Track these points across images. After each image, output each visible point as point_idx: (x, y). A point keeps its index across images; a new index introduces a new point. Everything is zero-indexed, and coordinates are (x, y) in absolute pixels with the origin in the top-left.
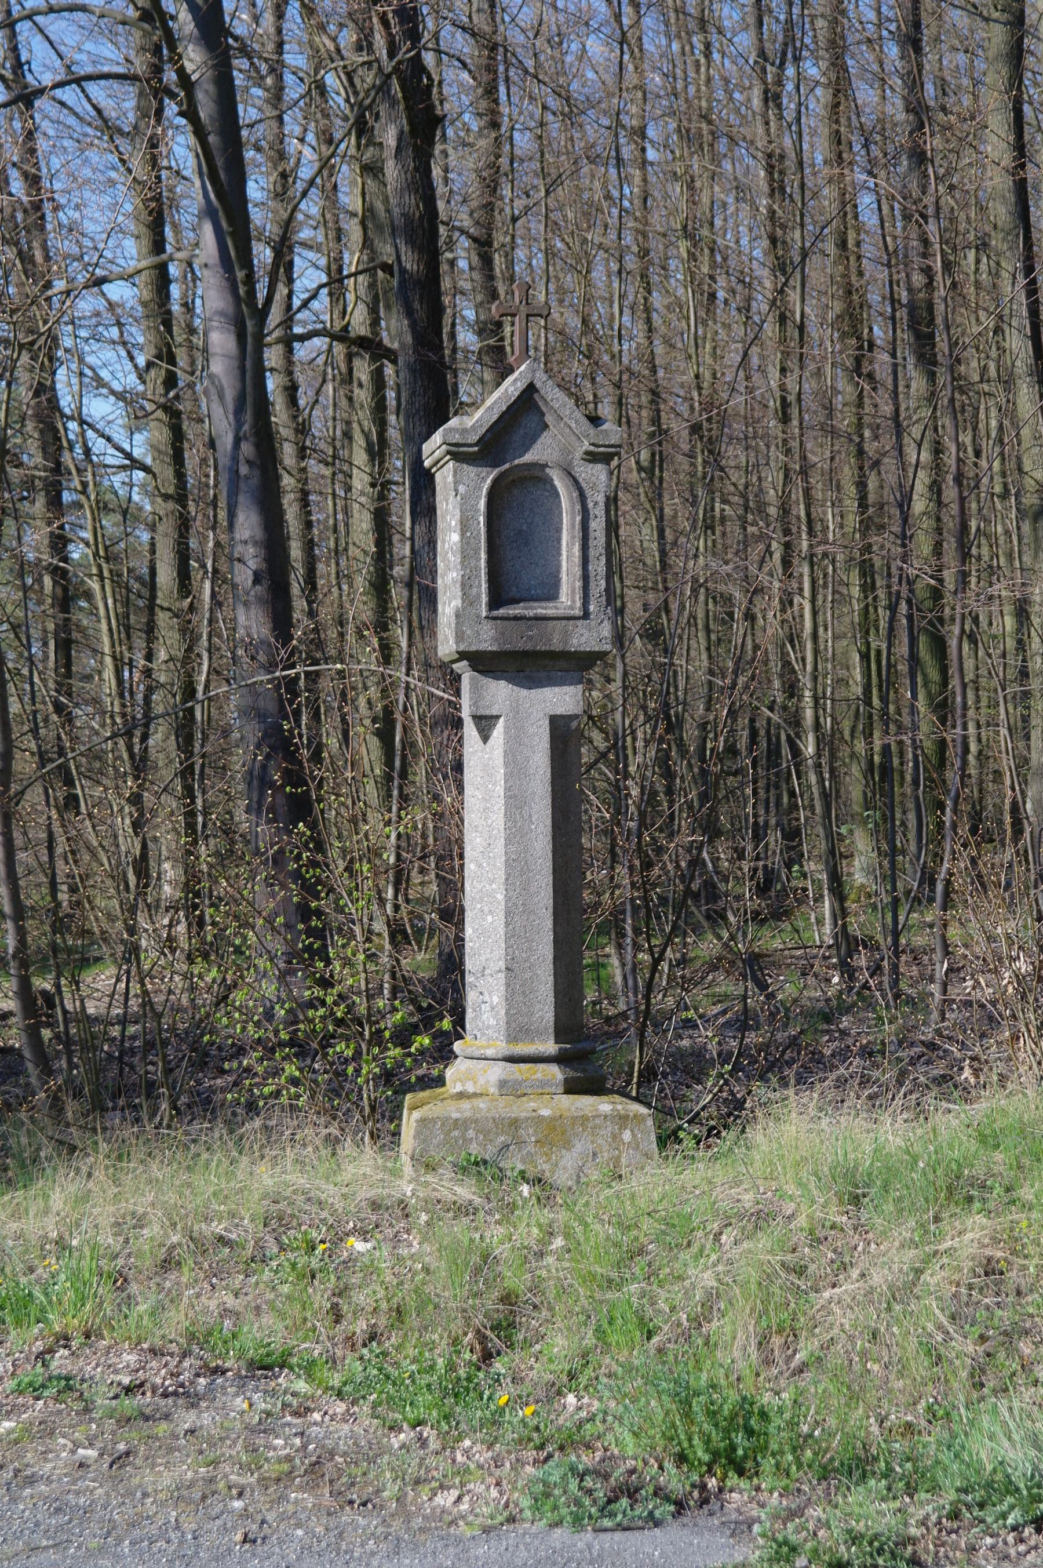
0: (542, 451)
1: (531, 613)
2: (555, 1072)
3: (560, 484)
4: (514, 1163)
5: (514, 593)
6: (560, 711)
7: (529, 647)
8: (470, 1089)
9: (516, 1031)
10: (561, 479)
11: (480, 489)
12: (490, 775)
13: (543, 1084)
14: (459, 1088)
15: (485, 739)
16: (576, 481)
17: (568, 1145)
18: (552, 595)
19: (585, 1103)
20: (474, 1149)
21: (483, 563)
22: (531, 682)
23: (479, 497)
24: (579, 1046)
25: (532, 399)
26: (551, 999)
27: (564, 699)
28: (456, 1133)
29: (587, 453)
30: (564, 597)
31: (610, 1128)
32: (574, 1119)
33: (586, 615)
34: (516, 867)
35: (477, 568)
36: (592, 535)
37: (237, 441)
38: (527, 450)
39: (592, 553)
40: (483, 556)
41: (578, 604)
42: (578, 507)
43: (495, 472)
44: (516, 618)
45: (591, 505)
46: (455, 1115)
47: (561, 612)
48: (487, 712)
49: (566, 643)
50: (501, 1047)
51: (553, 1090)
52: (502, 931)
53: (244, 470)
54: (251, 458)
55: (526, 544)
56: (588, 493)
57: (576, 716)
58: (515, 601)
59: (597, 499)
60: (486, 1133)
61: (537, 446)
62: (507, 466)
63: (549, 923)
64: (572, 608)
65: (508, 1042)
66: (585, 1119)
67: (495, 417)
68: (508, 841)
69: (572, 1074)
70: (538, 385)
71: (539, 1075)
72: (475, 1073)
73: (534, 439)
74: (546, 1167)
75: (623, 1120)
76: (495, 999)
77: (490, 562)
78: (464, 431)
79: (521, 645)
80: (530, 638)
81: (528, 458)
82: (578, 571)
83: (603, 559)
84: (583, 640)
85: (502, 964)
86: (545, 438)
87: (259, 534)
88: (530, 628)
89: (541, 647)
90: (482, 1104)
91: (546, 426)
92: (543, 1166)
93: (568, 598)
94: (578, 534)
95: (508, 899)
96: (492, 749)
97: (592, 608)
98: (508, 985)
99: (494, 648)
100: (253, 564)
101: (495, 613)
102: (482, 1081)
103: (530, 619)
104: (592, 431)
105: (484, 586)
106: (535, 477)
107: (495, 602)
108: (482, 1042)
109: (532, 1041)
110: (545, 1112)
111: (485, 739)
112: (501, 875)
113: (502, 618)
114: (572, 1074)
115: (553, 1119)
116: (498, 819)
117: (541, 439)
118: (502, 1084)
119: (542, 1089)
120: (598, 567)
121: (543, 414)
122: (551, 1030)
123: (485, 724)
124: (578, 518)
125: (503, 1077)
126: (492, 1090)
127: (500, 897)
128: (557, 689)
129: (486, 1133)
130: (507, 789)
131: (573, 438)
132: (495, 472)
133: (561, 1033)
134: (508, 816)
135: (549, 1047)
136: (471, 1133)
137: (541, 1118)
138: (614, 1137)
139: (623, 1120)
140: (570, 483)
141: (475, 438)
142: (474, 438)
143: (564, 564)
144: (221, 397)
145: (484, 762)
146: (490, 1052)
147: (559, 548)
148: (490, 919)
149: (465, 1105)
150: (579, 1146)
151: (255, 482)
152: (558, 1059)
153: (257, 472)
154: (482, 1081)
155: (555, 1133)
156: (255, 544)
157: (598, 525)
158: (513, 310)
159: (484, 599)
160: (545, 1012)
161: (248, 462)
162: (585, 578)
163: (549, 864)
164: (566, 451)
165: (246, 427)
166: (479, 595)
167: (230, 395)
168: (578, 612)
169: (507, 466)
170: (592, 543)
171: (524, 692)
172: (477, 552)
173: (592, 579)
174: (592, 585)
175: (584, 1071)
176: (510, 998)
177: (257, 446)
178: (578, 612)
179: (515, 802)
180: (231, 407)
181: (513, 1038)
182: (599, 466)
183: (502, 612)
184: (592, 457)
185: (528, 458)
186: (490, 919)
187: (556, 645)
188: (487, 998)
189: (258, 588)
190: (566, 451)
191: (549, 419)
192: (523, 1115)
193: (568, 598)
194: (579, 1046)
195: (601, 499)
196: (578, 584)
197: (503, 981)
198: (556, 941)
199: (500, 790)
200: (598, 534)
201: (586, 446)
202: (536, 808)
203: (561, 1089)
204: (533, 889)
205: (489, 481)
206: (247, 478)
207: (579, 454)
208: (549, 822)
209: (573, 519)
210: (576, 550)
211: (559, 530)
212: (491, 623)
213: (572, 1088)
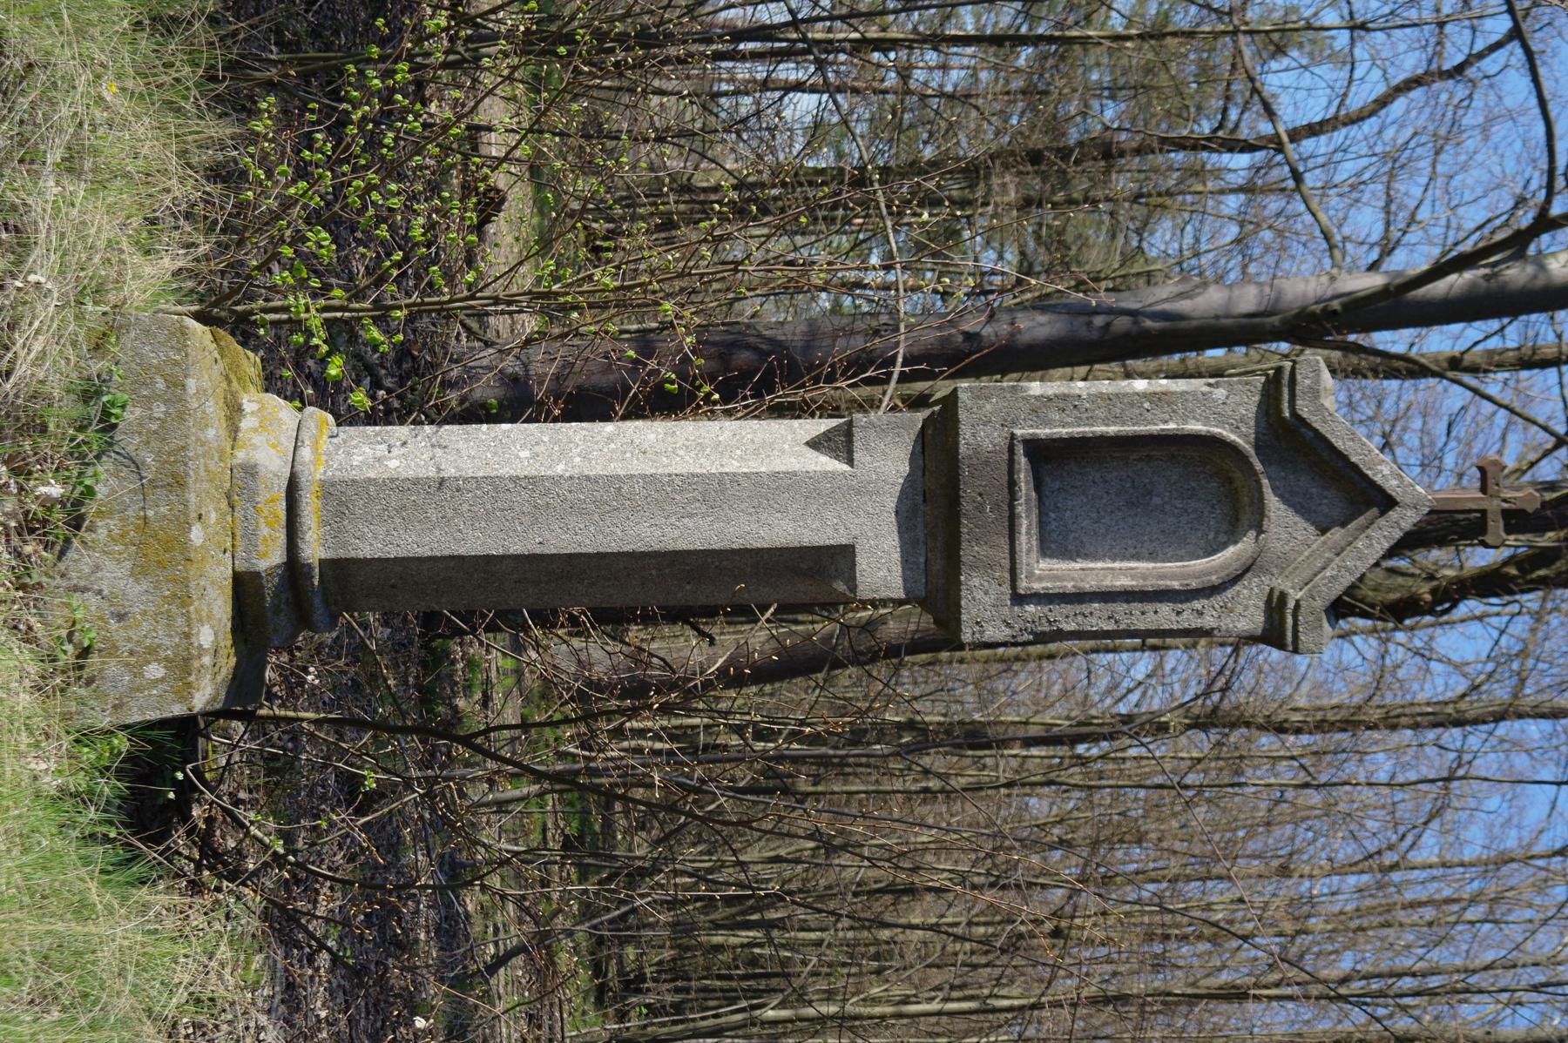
0: (1283, 523)
1: (1020, 509)
2: (271, 557)
3: (1230, 555)
4: (106, 481)
5: (1051, 484)
6: (862, 562)
7: (966, 506)
8: (246, 424)
9: (339, 496)
10: (1238, 556)
11: (1220, 424)
12: (756, 452)
13: (251, 536)
14: (248, 407)
15: (814, 444)
16: (1236, 579)
17: (139, 572)
18: (1046, 550)
19: (220, 606)
20: (132, 415)
21: (1100, 429)
22: (907, 515)
23: (1206, 422)
24: (317, 601)
25: (1368, 507)
26: (393, 553)
27: (881, 568)
28: (161, 384)
29: (1283, 596)
30: (1045, 565)
31: (168, 643)
32: (185, 583)
33: (1019, 599)
34: (608, 493)
35: (1091, 420)
36: (1149, 607)
37: (1133, 313)
38: (1285, 501)
39: (1120, 608)
40: (1112, 429)
41: (1037, 586)
42: (1194, 584)
43: (1249, 449)
44: (1012, 484)
45: (1197, 605)
46: (191, 384)
47: (1023, 558)
48: (857, 444)
49: (973, 567)
50: (314, 472)
51: (240, 553)
52: (505, 471)
53: (1099, 321)
54: (1112, 328)
55: (1131, 504)
56: (1217, 601)
57: (853, 588)
58: (1038, 486)
59: (1208, 614)
60: (160, 435)
61: (1292, 517)
62: (1259, 466)
63: (517, 548)
64: (1030, 576)
65: (323, 483)
66: (184, 600)
67: (1339, 444)
68: (649, 480)
69: (270, 586)
70: (1393, 515)
71: (265, 531)
72: (278, 435)
73: (1302, 510)
74: (102, 533)
75: (182, 667)
76: (393, 464)
77: (1103, 440)
78: (1315, 393)
79: (968, 494)
80: (980, 508)
81: (1272, 502)
82: (1090, 585)
83: (1109, 626)
84: (979, 595)
85: (450, 472)
86: (1303, 529)
87: (1025, 338)
88: (996, 507)
89: (966, 526)
90: (215, 432)
91: (1323, 531)
92: (103, 530)
93: (1044, 572)
94: (1150, 584)
95: (556, 480)
96: (799, 455)
97: (1031, 608)
98: (416, 481)
99: (962, 449)
100: (988, 331)
101: (1020, 449)
102: (257, 439)
103: (1012, 508)
104: (1320, 604)
105: (1064, 432)
106: (1240, 514)
107: (1040, 451)
108: (325, 444)
109: (324, 523)
110: (196, 535)
111: (814, 444)
112: (597, 470)
113: (1011, 461)
114: (270, 586)
115: (185, 545)
116: (685, 464)
117: (1302, 523)
118: (250, 470)
119: (240, 535)
120: (1098, 618)
121: (1343, 525)
122: (342, 554)
123: (840, 444)
124: (1176, 585)
125: (262, 472)
126: (241, 455)
127: (560, 469)
128: (897, 556)
129: (160, 435)
130: (734, 478)
131: (1307, 574)
132: (1249, 449)
133: (337, 568)
134: (691, 480)
135: (314, 550)
136: (159, 410)
137: (186, 527)
138: (152, 651)
139: (182, 667)
140: (1234, 569)
141: (1304, 413)
142: (1304, 409)
143: (1099, 565)
144: (1181, 296)
145: (776, 446)
146: (306, 453)
147: (1124, 558)
148: (525, 454)
149: (214, 409)
150: (135, 589)
151: (1083, 332)
152: (293, 565)
153: (1095, 335)
154: (257, 439)
155: (160, 551)
156: (1012, 335)
157: (1164, 616)
158: (1492, 488)
159: (1044, 432)
160: (371, 543)
161: (1108, 325)
162: (1079, 597)
163: (614, 547)
164: (1284, 564)
165: (1148, 323)
166: (1047, 423)
167: (1184, 306)
168: (1023, 585)
169: (1259, 466)
170: (1136, 607)
171: (891, 503)
172: (1118, 419)
173: (1078, 608)
174: (1068, 609)
175: (276, 610)
176: (396, 485)
177: (1127, 335)
178: (1023, 585)
179: (715, 490)
180: (1166, 306)
181: (329, 490)
182: (1260, 618)
183: (1022, 461)
184: (1275, 605)
185: (1272, 502)
186: (525, 454)
187: (970, 551)
188: (395, 452)
189: (960, 338)
190: (1284, 564)
191: (1337, 534)
192: (192, 498)
193: (1044, 572)
194: (317, 601)
195: (1208, 621)
196: (1069, 586)
197: (422, 474)
198: (488, 559)
199: (733, 466)
200: (1150, 616)
201: (1294, 595)
202: (704, 523)
203: (241, 566)
204: (572, 521)
205: (1233, 437)
206: (1089, 324)
207: (1281, 584)
208: (682, 545)
209: (1173, 577)
210: (1124, 582)
211: (1152, 557)
212: (1004, 444)
213: (244, 586)
